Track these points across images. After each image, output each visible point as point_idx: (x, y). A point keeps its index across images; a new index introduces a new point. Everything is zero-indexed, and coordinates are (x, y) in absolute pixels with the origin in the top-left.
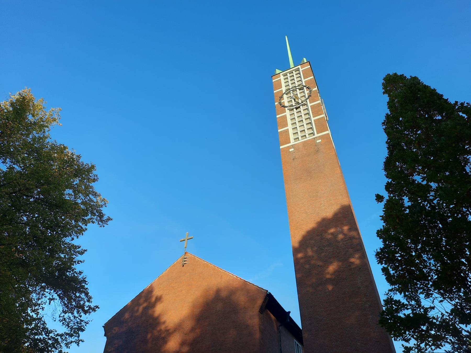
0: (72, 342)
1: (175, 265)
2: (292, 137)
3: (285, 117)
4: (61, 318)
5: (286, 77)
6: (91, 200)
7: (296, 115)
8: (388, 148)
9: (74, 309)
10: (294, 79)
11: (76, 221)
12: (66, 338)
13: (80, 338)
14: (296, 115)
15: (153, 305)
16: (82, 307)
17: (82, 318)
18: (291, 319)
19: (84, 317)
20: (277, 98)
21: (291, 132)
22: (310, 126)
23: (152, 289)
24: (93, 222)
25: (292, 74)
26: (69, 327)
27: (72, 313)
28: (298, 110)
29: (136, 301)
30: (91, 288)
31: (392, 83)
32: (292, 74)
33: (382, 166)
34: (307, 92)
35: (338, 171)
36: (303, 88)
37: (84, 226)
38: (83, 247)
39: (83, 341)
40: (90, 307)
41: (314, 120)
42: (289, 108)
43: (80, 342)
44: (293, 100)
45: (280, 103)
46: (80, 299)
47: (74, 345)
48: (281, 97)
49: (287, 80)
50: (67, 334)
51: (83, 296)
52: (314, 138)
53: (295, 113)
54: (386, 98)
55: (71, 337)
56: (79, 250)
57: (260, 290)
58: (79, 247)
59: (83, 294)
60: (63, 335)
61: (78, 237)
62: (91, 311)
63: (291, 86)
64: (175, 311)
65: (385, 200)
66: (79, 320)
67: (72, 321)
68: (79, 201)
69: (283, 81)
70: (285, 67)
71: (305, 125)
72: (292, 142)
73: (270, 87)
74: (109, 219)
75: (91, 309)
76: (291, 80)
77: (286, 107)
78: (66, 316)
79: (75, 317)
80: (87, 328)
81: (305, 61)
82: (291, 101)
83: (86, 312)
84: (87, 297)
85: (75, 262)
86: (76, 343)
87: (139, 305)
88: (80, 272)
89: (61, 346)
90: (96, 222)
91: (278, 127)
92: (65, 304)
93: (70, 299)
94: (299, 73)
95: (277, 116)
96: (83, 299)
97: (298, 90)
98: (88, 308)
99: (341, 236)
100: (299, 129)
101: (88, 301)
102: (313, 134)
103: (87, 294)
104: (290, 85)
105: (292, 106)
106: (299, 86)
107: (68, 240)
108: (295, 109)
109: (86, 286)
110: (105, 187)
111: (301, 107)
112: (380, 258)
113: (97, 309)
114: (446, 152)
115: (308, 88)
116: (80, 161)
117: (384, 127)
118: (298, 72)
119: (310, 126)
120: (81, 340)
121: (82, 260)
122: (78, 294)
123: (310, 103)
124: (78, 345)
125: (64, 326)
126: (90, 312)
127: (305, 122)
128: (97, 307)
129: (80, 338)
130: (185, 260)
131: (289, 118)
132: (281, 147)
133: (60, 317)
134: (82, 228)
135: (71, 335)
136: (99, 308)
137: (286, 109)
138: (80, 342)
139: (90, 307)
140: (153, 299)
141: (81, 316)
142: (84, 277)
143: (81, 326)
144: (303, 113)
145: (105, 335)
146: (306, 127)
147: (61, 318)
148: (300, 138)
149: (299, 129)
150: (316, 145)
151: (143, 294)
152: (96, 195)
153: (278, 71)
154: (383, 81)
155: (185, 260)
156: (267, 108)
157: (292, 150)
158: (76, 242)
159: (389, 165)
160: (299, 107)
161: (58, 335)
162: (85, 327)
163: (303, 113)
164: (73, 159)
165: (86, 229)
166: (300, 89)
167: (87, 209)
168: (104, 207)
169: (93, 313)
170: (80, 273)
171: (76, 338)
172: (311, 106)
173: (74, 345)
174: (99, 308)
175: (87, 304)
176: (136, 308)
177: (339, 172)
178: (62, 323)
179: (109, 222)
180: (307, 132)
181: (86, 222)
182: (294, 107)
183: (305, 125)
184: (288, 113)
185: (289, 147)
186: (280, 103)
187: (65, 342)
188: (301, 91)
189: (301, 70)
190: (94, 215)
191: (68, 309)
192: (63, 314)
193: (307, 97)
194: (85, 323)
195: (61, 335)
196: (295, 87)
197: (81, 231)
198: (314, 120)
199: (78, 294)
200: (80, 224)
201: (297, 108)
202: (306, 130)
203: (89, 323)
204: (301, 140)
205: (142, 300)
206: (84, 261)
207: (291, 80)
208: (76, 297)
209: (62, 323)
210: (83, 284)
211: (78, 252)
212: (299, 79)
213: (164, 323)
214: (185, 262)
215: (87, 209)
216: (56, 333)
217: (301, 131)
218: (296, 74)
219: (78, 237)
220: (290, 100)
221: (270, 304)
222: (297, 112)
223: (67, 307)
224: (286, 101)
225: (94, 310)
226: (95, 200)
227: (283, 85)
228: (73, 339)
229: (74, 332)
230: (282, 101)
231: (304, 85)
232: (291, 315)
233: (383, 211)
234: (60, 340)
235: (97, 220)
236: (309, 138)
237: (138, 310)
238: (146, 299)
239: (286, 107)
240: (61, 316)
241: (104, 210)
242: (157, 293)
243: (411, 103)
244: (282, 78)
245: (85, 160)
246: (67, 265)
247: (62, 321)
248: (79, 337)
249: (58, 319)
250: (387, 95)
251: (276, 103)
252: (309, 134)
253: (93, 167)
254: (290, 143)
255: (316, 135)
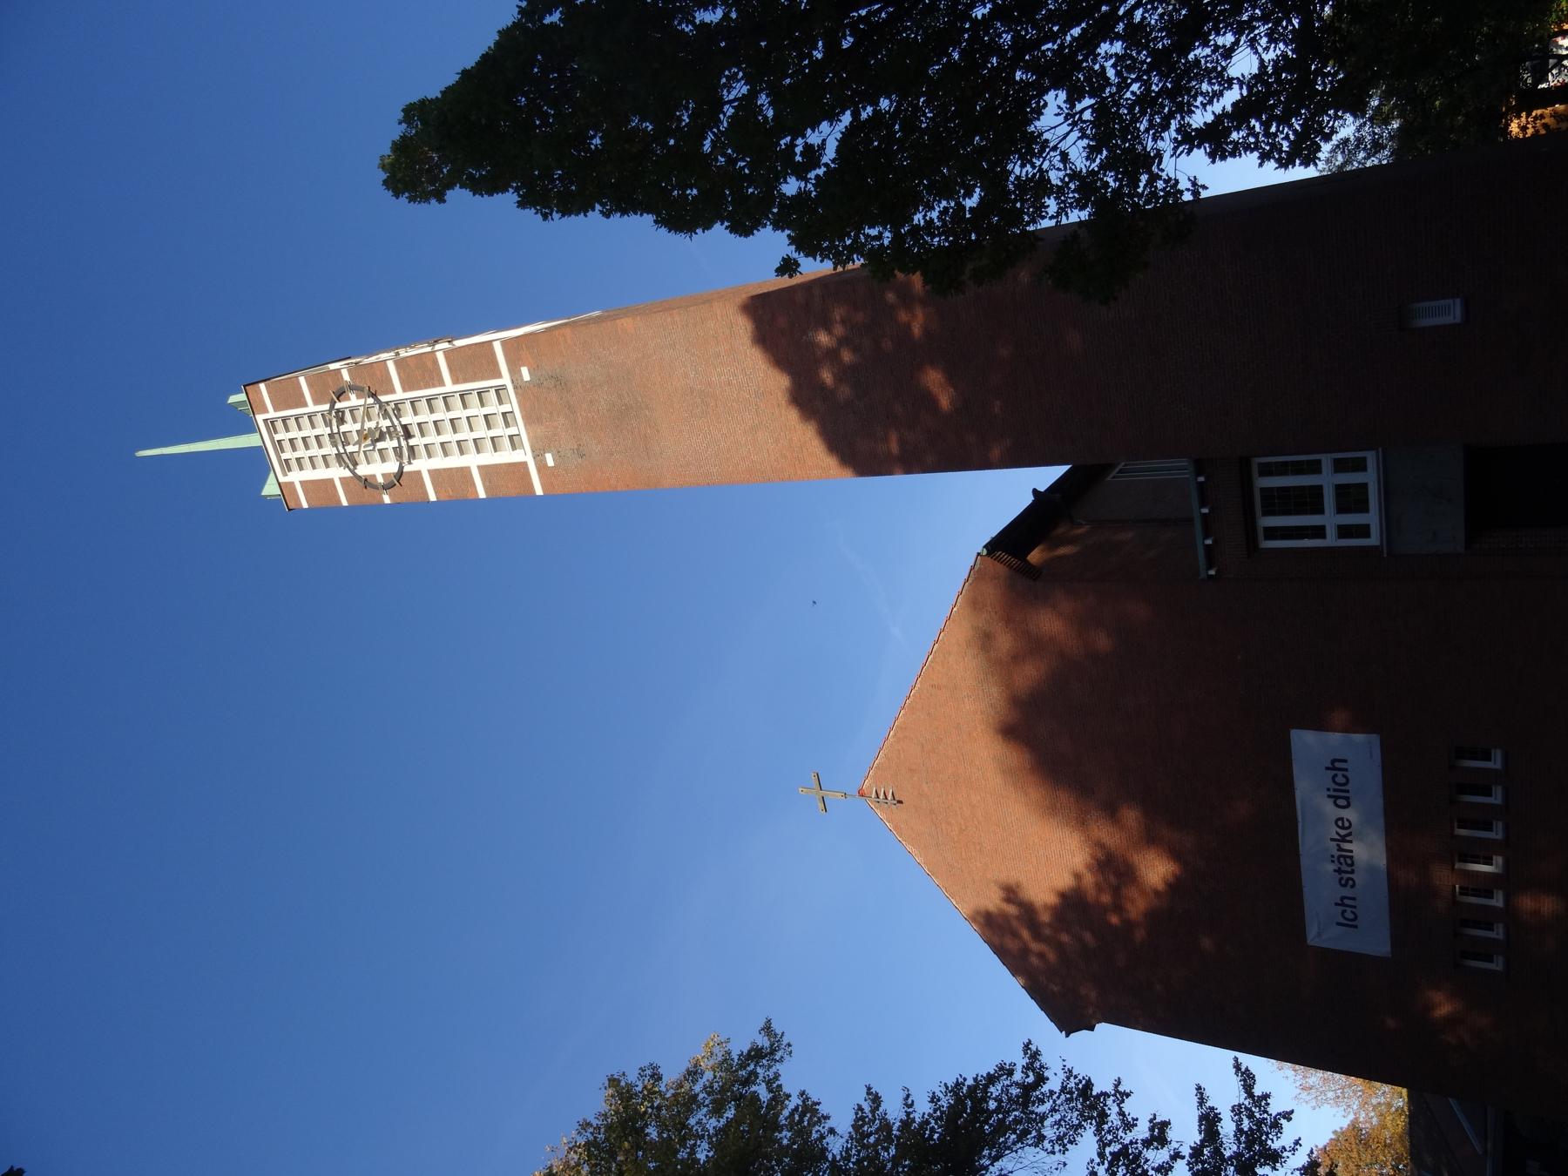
0: (1121, 1113)
2: (507, 456)
4: (1057, 1148)
5: (294, 464)
6: (709, 1089)
10: (291, 441)
13: (1110, 1089)
14: (432, 438)
15: (1028, 911)
16: (1027, 1089)
17: (1057, 1089)
19: (1054, 1084)
20: (367, 496)
21: (489, 458)
23: (978, 913)
24: (777, 1076)
25: (286, 445)
27: (1043, 1117)
28: (415, 430)
29: (1015, 961)
32: (286, 445)
34: (353, 400)
36: (338, 411)
38: (860, 1097)
39: (1119, 1082)
42: (405, 460)
43: (1121, 1089)
44: (380, 445)
45: (388, 487)
46: (1005, 1098)
47: (1126, 1107)
48: (367, 482)
49: (307, 462)
50: (1099, 1130)
51: (994, 1090)
52: (515, 388)
54: (458, 196)
55: (1107, 1116)
56: (867, 1109)
58: (860, 1108)
61: (827, 1118)
62: (1037, 1064)
63: (329, 450)
64: (1050, 856)
69: (309, 474)
70: (257, 462)
71: (469, 412)
72: (524, 455)
74: (767, 1029)
76: (304, 447)
77: (401, 467)
78: (1049, 1132)
79: (1053, 1110)
80: (1081, 1071)
81: (242, 397)
82: (380, 451)
83: (1041, 1079)
84: (998, 1078)
87: (1025, 951)
90: (773, 1069)
92: (1021, 1138)
93: (1001, 1128)
94: (285, 420)
96: (1005, 1090)
97: (343, 428)
99: (847, 356)
100: (481, 431)
101: (1010, 1073)
102: (499, 391)
103: (991, 1079)
105: (398, 452)
106: (328, 424)
107: (835, 1146)
108: (412, 442)
109: (970, 1082)
110: (679, 1042)
111: (404, 421)
115: (340, 395)
116: (595, 1122)
118: (279, 424)
120: (1116, 1086)
122: (992, 1105)
123: (393, 391)
124: (1128, 1095)
126: (1042, 1066)
127: (458, 412)
128: (1027, 1047)
129: (1110, 1089)
131: (440, 462)
132: (539, 491)
134: (796, 1109)
135: (1103, 1116)
137: (407, 468)
138: (1121, 1089)
140: (1012, 910)
141: (1052, 1092)
144: (425, 416)
146: (475, 410)
147: (1057, 1148)
148: (512, 431)
149: (481, 431)
150: (536, 383)
151: (996, 940)
153: (270, 489)
154: (403, 199)
156: (394, 532)
157: (550, 460)
158: (842, 1121)
160: (405, 427)
161: (1101, 1155)
163: (425, 416)
164: (588, 1144)
166: (341, 421)
169: (1044, 1059)
170: (934, 1099)
171: (1110, 1101)
172: (405, 390)
173: (1126, 1107)
175: (1018, 1076)
176: (1034, 960)
179: (777, 1027)
180: (492, 407)
181: (778, 1097)
182: (403, 443)
183: (469, 412)
184: (422, 465)
185: (542, 466)
186: (388, 487)
187: (1121, 1133)
188: (348, 416)
189: (272, 414)
190: (754, 1074)
191: (1028, 1130)
192: (1047, 1144)
193: (370, 401)
195: (1103, 1145)
196: (331, 436)
197: (809, 1108)
199: (992, 1105)
200: (786, 1113)
201: (408, 435)
202: (486, 410)
203: (1069, 1066)
204: (520, 428)
205: (1011, 944)
207: (304, 447)
208: (998, 1110)
211: (873, 1112)
213: (1078, 876)
216: (1097, 1160)
218: (287, 430)
219: (827, 1118)
220: (376, 455)
222: (423, 435)
224: (378, 469)
225: (1035, 1055)
226: (709, 1075)
227: (321, 474)
228: (1113, 1111)
231: (327, 407)
234: (1115, 1147)
235: (770, 1067)
236: (513, 405)
237: (1041, 956)
238: (1012, 932)
239: (401, 467)
241: (740, 1047)
242: (993, 901)
243: (482, 137)
244: (295, 477)
245: (596, 1104)
246: (912, 1136)
248: (1106, 1095)
249: (1058, 1157)
251: (387, 499)
252: (501, 402)
253: (613, 1082)
255: (506, 380)
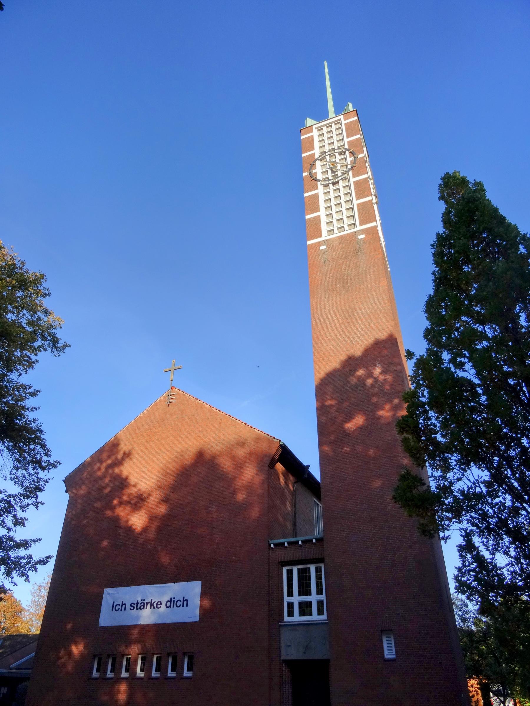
0: (28, 505)
1: (157, 404)
2: (324, 228)
3: (316, 196)
4: (13, 476)
5: (321, 132)
6: (39, 319)
7: (333, 194)
8: (435, 281)
9: (29, 465)
11: (22, 350)
12: (20, 499)
16: (39, 462)
18: (310, 474)
19: (42, 474)
20: (306, 165)
21: (324, 220)
22: (350, 213)
25: (329, 129)
26: (23, 486)
27: (26, 470)
28: (336, 187)
30: (49, 438)
31: (451, 185)
32: (329, 129)
33: (422, 306)
34: (350, 159)
35: (385, 282)
36: (345, 152)
37: (34, 358)
38: (35, 387)
40: (49, 463)
41: (358, 205)
42: (323, 183)
43: (39, 505)
44: (329, 171)
47: (31, 507)
50: (21, 495)
51: (39, 448)
52: (355, 232)
53: (332, 192)
55: (27, 499)
57: (271, 440)
58: (30, 387)
59: (39, 446)
60: (16, 496)
61: (26, 372)
62: (50, 467)
63: (327, 148)
65: (415, 358)
66: (36, 479)
67: (26, 479)
68: (24, 321)
70: (321, 115)
71: (344, 211)
73: (297, 146)
74: (66, 346)
75: (51, 465)
76: (329, 135)
77: (319, 181)
78: (20, 472)
79: (30, 474)
80: (47, 487)
81: (351, 109)
83: (43, 469)
85: (28, 409)
86: (34, 506)
88: (34, 420)
89: (15, 509)
90: (48, 348)
91: (306, 213)
95: (306, 195)
97: (337, 155)
98: (46, 464)
100: (335, 217)
101: (46, 455)
102: (354, 224)
103: (44, 446)
104: (327, 146)
105: (326, 179)
106: (339, 148)
108: (331, 185)
111: (340, 182)
112: (401, 428)
113: (58, 465)
114: (490, 303)
115: (352, 153)
117: (433, 250)
118: (339, 126)
119: (350, 213)
120: (41, 503)
121: (37, 407)
122: (32, 447)
123: (354, 177)
124: (36, 508)
125: (17, 485)
126: (49, 469)
127: (344, 206)
128: (58, 462)
129: (39, 500)
130: (171, 397)
132: (309, 243)
133: (10, 474)
134: (30, 358)
135: (27, 497)
136: (60, 464)
137: (319, 183)
138: (39, 505)
139: (48, 463)
141: (38, 474)
142: (39, 425)
143: (39, 485)
144: (342, 191)
145: (67, 491)
147: (13, 476)
149: (335, 217)
150: (357, 242)
152: (46, 313)
153: (310, 122)
154: (440, 182)
155: (171, 397)
156: (292, 175)
158: (25, 379)
159: (431, 307)
160: (337, 182)
161: (10, 496)
162: (45, 486)
163: (342, 191)
164: (14, 265)
165: (37, 361)
166: (340, 154)
167: (35, 332)
168: (59, 329)
169: (53, 470)
171: (34, 500)
173: (31, 507)
174: (60, 464)
175: (45, 458)
177: (386, 283)
178: (14, 481)
179: (67, 350)
180: (346, 222)
182: (330, 182)
183: (344, 211)
184: (320, 190)
185: (319, 244)
187: (19, 504)
188: (342, 157)
189: (343, 122)
193: (349, 167)
194: (44, 481)
195: (14, 497)
197: (31, 364)
198: (358, 205)
201: (334, 184)
203: (50, 481)
204: (337, 234)
206: (39, 408)
207: (329, 135)
208: (30, 449)
209: (14, 481)
210: (39, 434)
211: (29, 393)
212: (340, 137)
214: (171, 401)
215: (35, 332)
216: (7, 494)
217: (338, 220)
218: (336, 129)
219: (26, 372)
221: (286, 456)
222: (334, 190)
223: (20, 462)
224: (319, 171)
225: (54, 466)
226: (45, 319)
227: (317, 144)
229: (31, 492)
230: (314, 171)
231: (347, 147)
232: (310, 469)
233: (412, 370)
235: (49, 347)
236: (348, 231)
239: (319, 181)
240: (12, 473)
241: (59, 333)
244: (315, 133)
245: (32, 269)
247: (14, 479)
248: (37, 498)
249: (9, 477)
250: (443, 202)
254: (321, 236)
255: (359, 228)
